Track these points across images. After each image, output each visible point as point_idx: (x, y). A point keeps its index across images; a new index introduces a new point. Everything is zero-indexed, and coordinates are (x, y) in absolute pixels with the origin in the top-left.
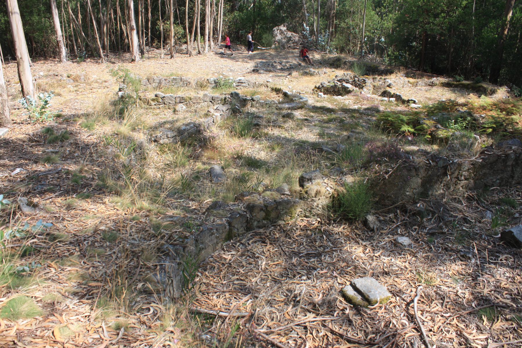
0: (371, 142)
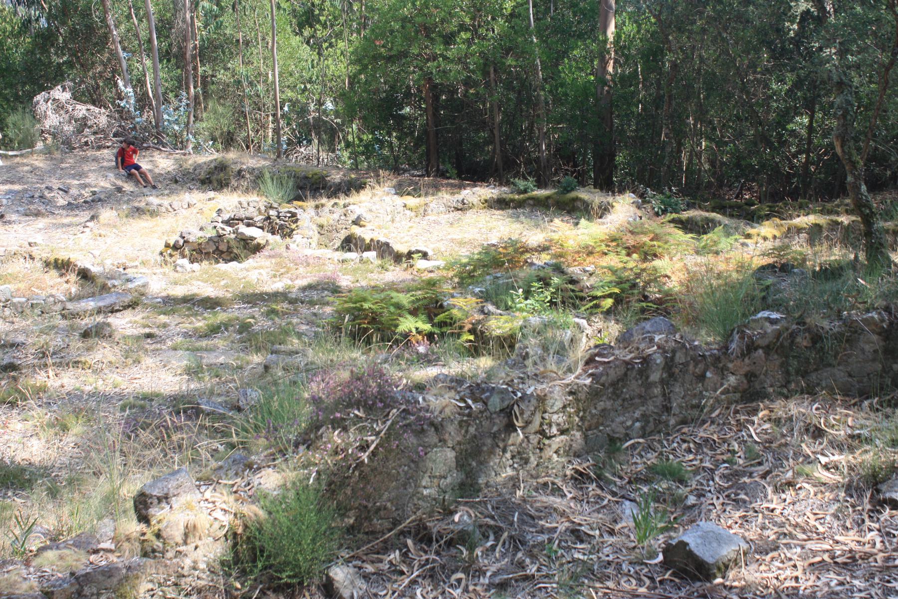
0: (325, 372)
